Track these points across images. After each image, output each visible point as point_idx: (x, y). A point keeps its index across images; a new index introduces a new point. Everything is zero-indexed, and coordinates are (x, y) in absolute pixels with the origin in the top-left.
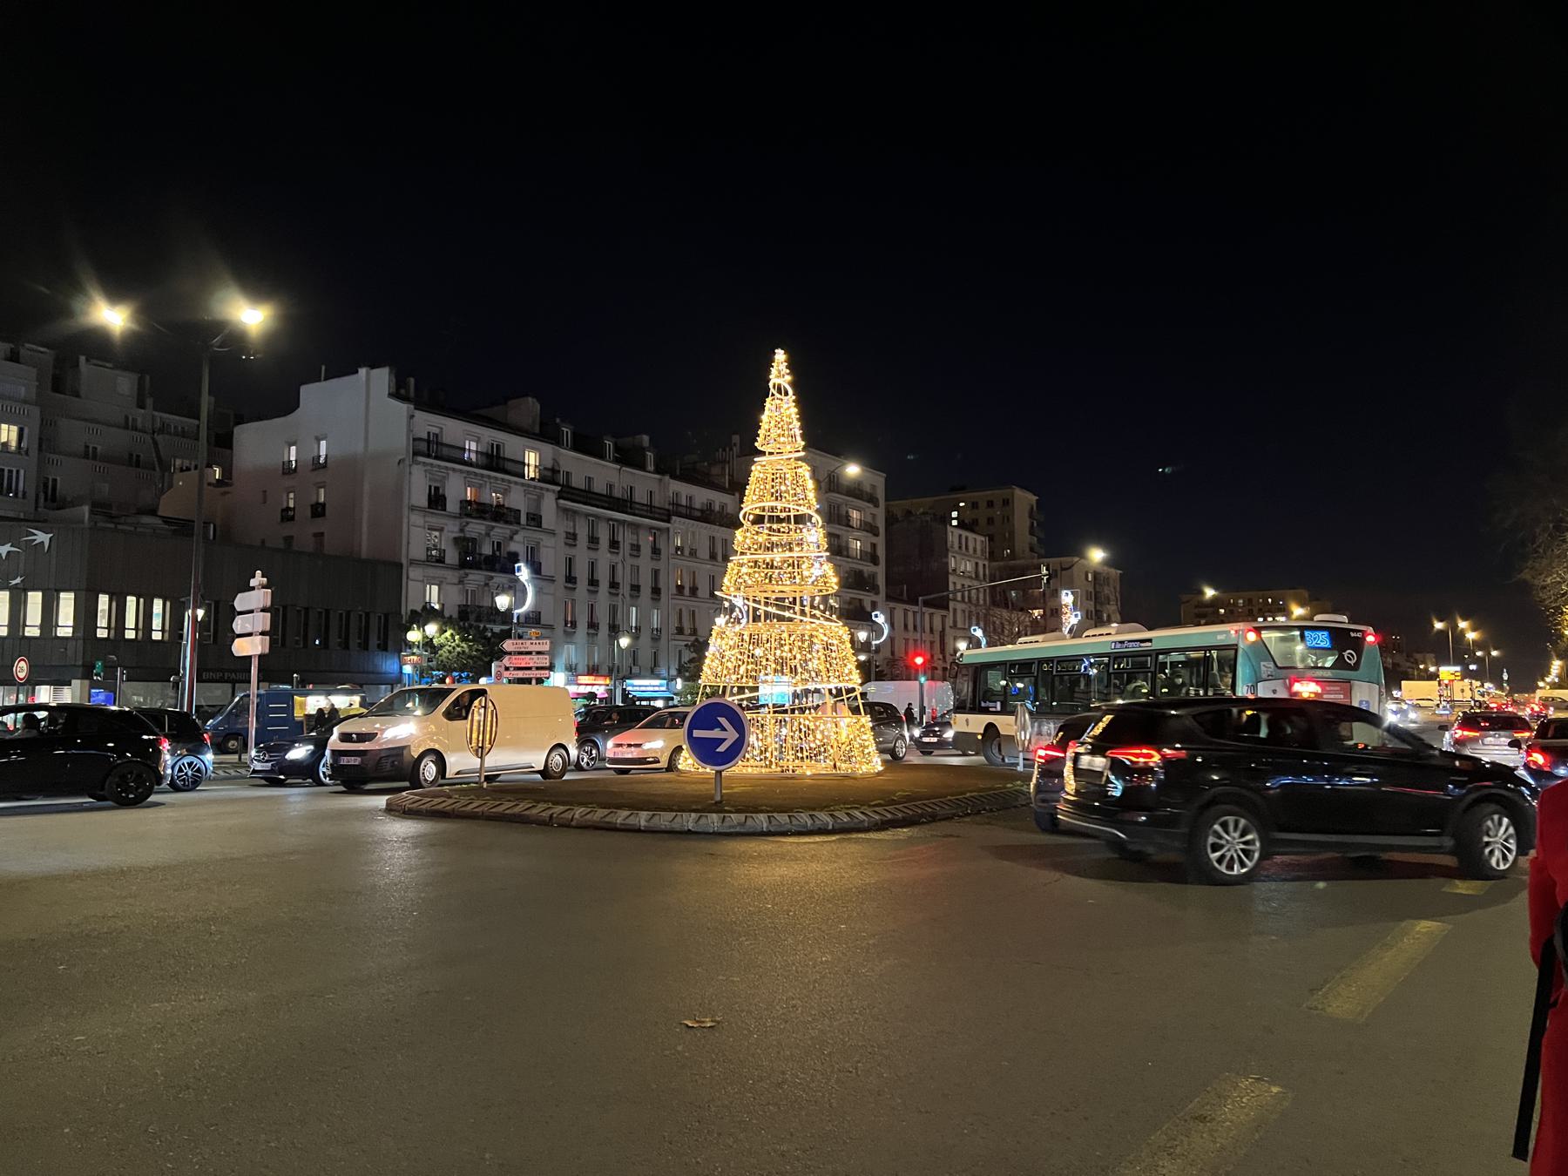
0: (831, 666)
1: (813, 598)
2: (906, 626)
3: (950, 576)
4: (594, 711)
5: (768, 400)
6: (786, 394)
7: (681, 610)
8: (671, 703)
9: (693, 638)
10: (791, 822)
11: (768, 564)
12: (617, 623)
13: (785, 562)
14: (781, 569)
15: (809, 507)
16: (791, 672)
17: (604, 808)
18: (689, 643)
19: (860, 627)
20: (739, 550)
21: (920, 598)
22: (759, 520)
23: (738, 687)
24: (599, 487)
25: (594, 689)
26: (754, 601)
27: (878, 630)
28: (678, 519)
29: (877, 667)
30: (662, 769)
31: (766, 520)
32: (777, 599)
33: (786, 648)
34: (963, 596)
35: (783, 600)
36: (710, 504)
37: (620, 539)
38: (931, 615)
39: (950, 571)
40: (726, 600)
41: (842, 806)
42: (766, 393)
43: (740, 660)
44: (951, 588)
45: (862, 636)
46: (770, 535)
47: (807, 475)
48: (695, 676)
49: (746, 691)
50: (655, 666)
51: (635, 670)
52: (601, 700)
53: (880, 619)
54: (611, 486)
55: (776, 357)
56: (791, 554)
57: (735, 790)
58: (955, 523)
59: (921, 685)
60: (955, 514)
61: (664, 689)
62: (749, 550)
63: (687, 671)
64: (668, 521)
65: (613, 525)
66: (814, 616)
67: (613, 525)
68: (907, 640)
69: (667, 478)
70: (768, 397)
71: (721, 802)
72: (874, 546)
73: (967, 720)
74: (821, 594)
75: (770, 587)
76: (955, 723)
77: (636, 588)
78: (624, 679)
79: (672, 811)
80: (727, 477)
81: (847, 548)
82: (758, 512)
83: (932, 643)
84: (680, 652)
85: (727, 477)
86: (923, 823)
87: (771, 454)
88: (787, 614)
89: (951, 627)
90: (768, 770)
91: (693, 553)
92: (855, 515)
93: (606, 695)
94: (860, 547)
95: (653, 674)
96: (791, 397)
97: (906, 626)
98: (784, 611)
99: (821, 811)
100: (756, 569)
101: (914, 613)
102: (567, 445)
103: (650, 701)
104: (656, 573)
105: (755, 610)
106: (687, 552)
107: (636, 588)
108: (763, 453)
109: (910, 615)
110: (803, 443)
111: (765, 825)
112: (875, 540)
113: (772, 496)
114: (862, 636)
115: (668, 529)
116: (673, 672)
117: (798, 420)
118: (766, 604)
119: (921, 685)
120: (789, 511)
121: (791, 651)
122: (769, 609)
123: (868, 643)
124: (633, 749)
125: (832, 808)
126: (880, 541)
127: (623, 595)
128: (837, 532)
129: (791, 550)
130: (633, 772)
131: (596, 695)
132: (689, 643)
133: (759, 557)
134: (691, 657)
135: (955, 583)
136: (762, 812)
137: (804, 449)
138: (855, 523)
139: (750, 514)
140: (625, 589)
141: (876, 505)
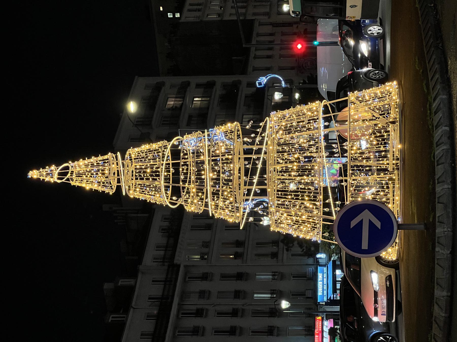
0: (305, 127)
1: (244, 143)
2: (269, 57)
3: (224, 19)
4: (346, 337)
5: (73, 183)
6: (67, 168)
7: (256, 255)
8: (338, 263)
9: (281, 245)
10: (443, 163)
11: (215, 183)
12: (268, 310)
13: (213, 168)
14: (219, 171)
15: (165, 147)
16: (311, 161)
17: (432, 327)
18: (285, 247)
19: (269, 97)
20: (203, 208)
21: (244, 46)
22: (176, 192)
23: (324, 207)
24: (149, 326)
25: (326, 329)
26: (248, 194)
27: (273, 82)
28: (176, 258)
29: (304, 83)
30: (396, 273)
31: (177, 185)
32: (246, 175)
33: (290, 166)
34: (242, 7)
35: (247, 171)
36: (163, 229)
37: (194, 308)
38: (258, 35)
39: (219, 19)
40: (247, 219)
41: (429, 118)
42: (67, 186)
43: (300, 207)
44: (235, 18)
45: (278, 96)
46: (190, 182)
47: (136, 149)
48: (315, 244)
49: (327, 201)
50: (305, 277)
51: (309, 294)
52: (335, 324)
53: (264, 80)
54: (149, 316)
55: (35, 177)
56: (207, 162)
57: (415, 211)
58: (178, 15)
59: (321, 44)
60: (170, 15)
61: (325, 269)
62: (203, 199)
63: (310, 249)
64: (179, 266)
65: (183, 314)
66: (261, 143)
67: (183, 314)
68: (281, 56)
69: (141, 267)
70: (70, 184)
71: (426, 225)
72: (198, 86)
73: (352, 7)
74: (241, 136)
75: (236, 182)
76: (354, 17)
77: (237, 294)
78: (317, 304)
79: (433, 268)
80: (139, 215)
81: (200, 109)
82: (169, 192)
83: (283, 34)
84: (293, 255)
85: (139, 215)
86: (443, 46)
87: (119, 181)
88: (260, 166)
89: (269, 18)
90: (396, 182)
91: (206, 245)
92: (171, 103)
93: (332, 320)
94: (198, 97)
95: (314, 278)
96: (70, 164)
97: (269, 57)
98: (257, 168)
99: (433, 137)
100: (220, 193)
101: (256, 50)
102: (124, 317)
103: (336, 281)
104: (224, 277)
105: (256, 194)
106: (205, 250)
107: (237, 294)
108: (119, 188)
109: (259, 53)
110: (110, 154)
111: (446, 186)
112: (193, 85)
113: (156, 180)
114: (278, 96)
115: (186, 266)
116: (311, 261)
117: (89, 158)
118: (251, 184)
119: (321, 44)
120: (169, 164)
121: (291, 162)
122: (255, 181)
123: (283, 91)
124: (379, 299)
125: (430, 127)
126: (194, 80)
127: (243, 305)
128: (186, 116)
129: (203, 162)
130: (399, 299)
131: (331, 328)
132: (285, 247)
133: (209, 189)
134: (297, 246)
135: (231, 15)
136: (434, 189)
137: (115, 153)
138: (179, 103)
139: (171, 199)
140: (238, 303)
141: (163, 84)
